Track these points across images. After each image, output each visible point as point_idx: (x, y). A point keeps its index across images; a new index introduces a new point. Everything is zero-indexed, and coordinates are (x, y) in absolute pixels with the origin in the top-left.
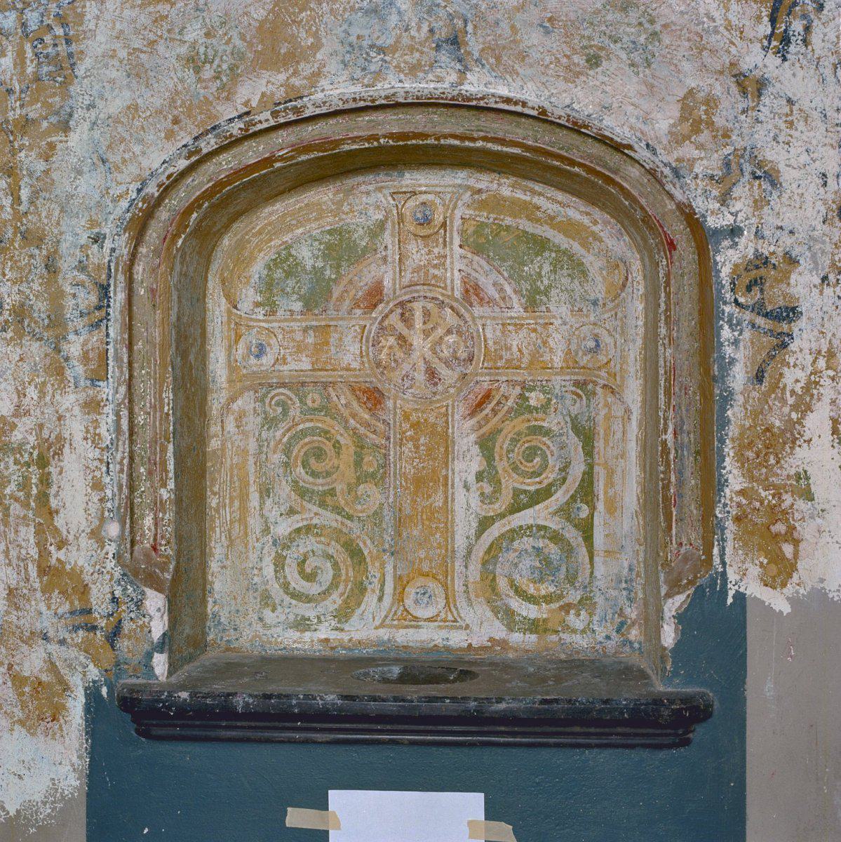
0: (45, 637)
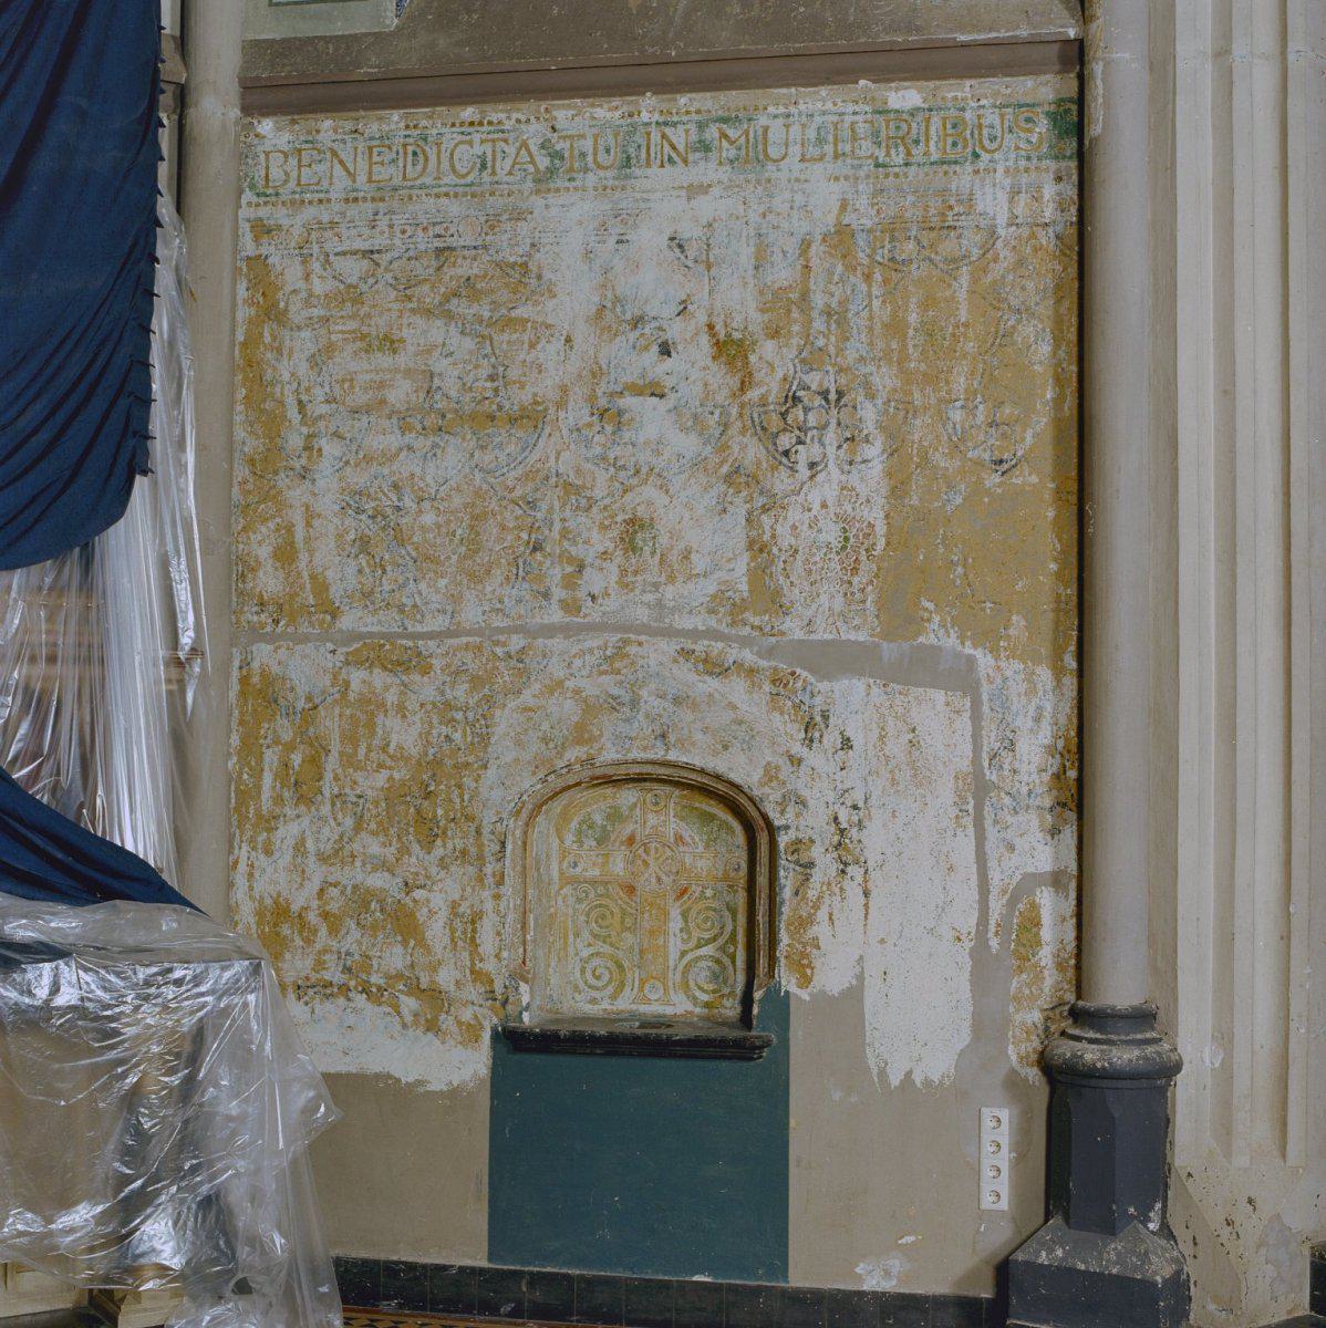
0: (473, 1003)
